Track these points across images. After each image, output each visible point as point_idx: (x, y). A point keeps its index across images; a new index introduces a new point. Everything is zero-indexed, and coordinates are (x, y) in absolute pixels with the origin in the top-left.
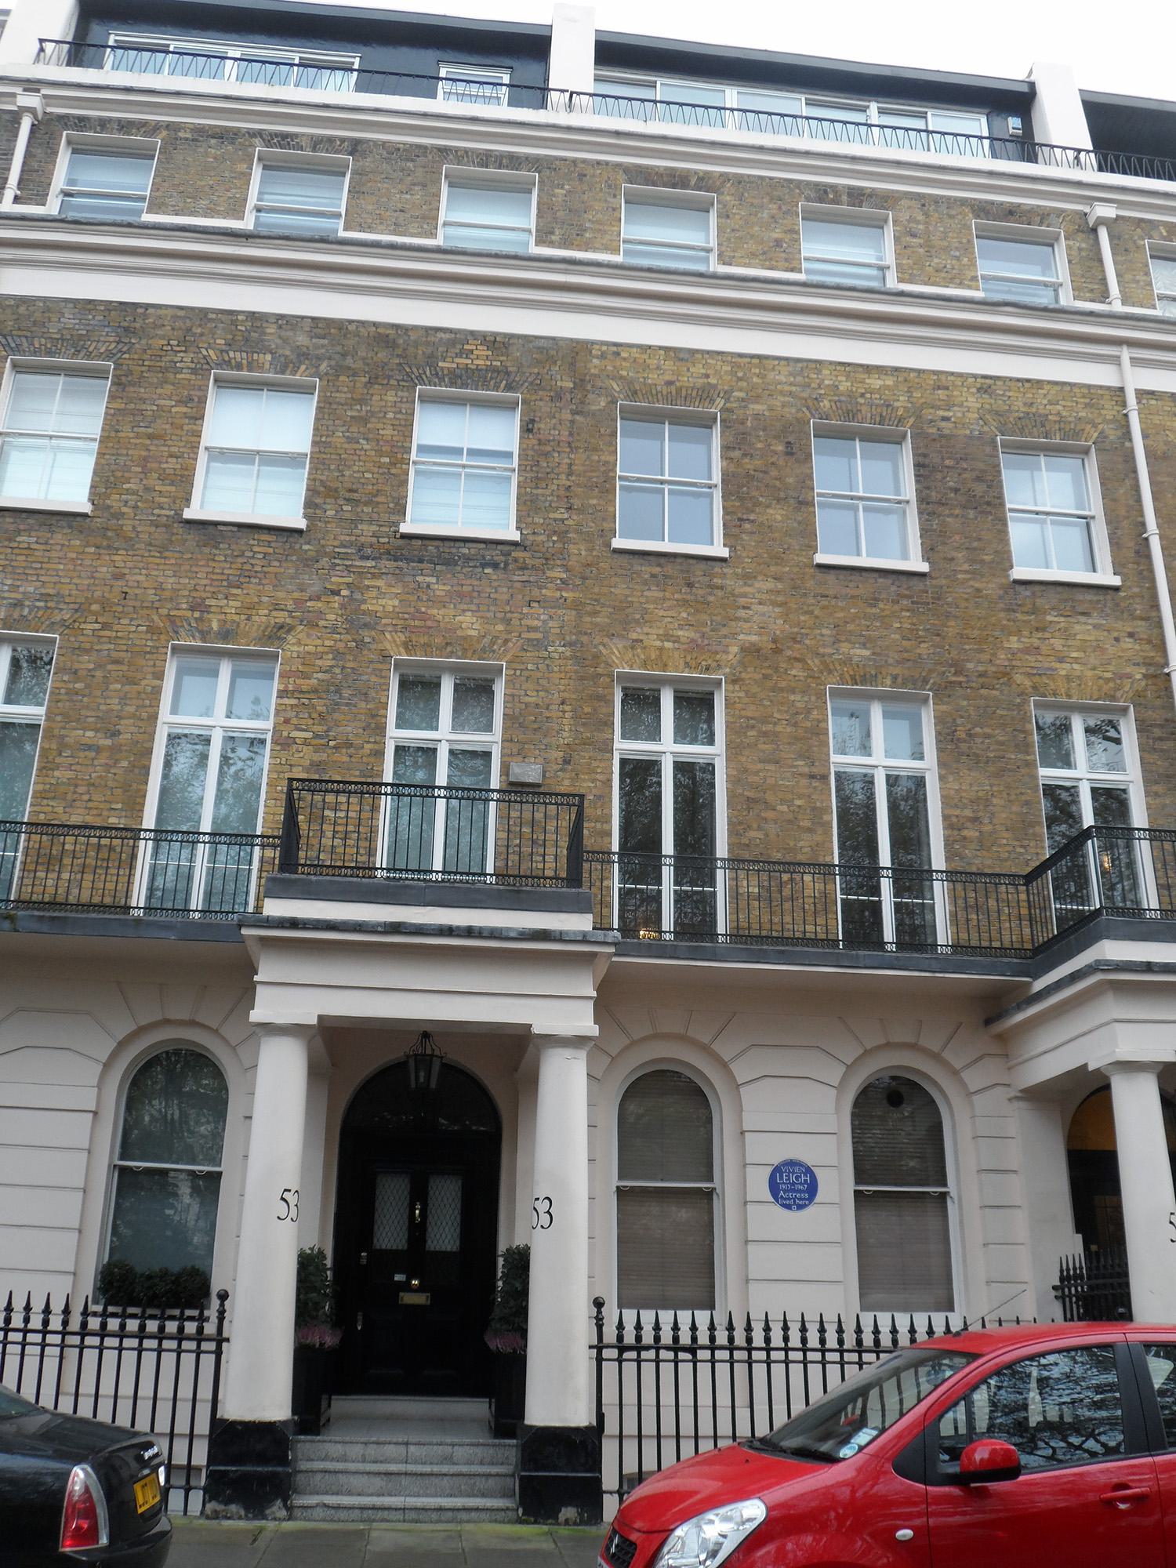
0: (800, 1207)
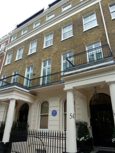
0: (55, 116)
